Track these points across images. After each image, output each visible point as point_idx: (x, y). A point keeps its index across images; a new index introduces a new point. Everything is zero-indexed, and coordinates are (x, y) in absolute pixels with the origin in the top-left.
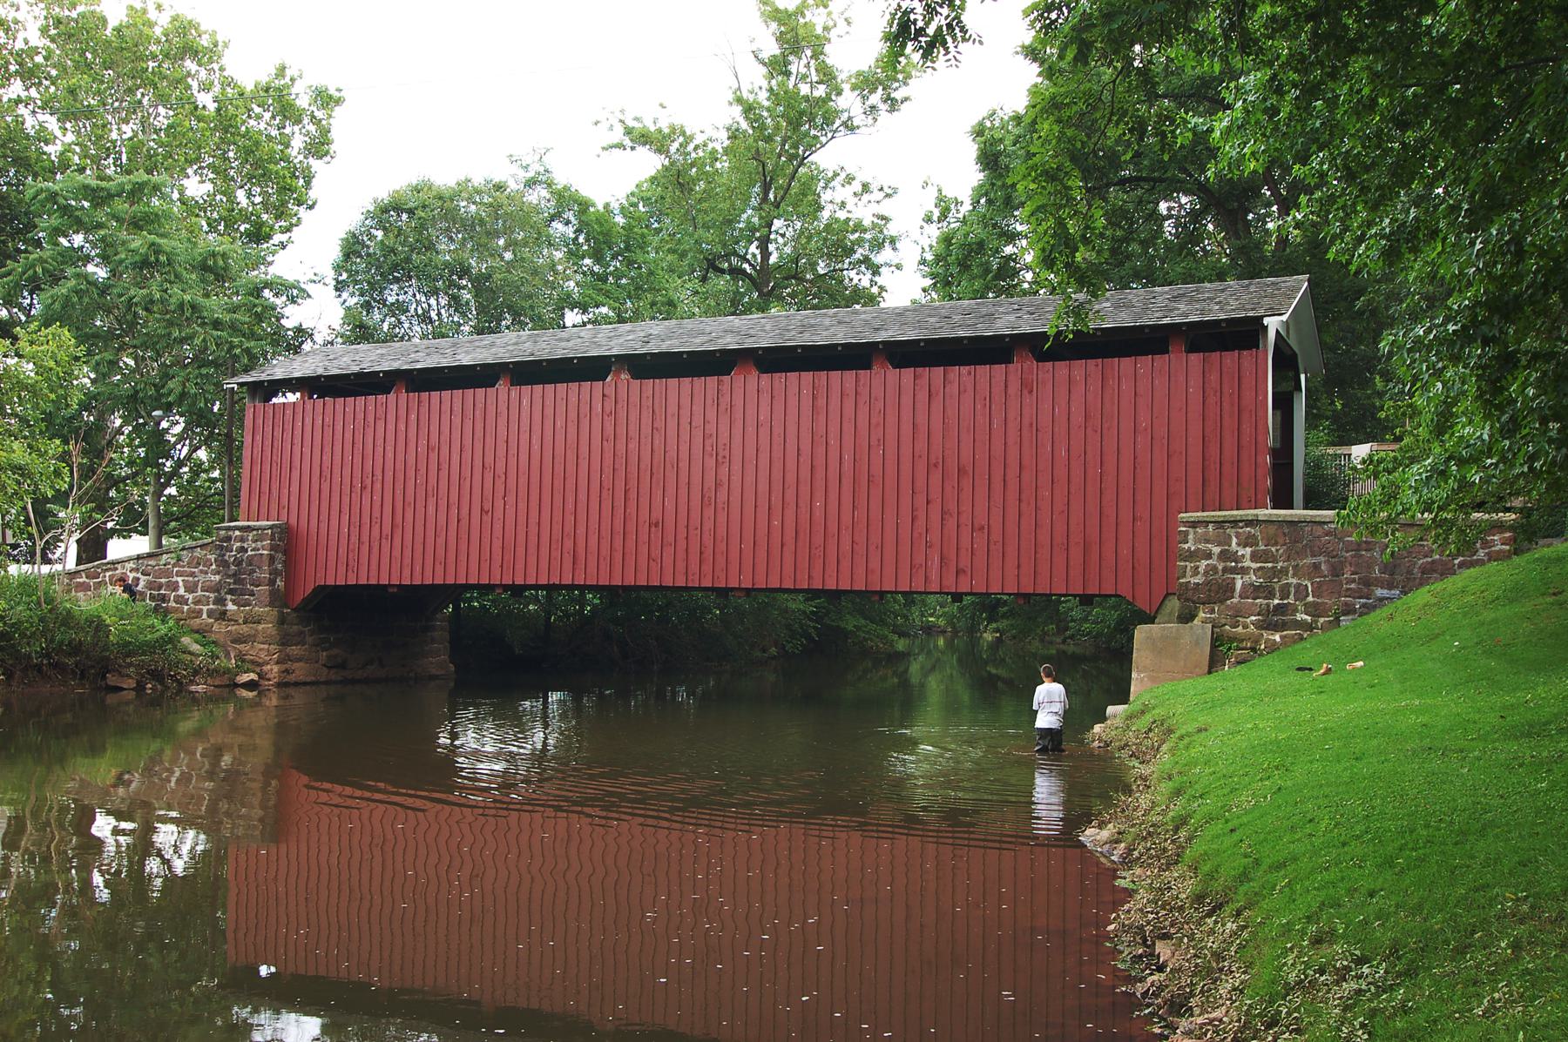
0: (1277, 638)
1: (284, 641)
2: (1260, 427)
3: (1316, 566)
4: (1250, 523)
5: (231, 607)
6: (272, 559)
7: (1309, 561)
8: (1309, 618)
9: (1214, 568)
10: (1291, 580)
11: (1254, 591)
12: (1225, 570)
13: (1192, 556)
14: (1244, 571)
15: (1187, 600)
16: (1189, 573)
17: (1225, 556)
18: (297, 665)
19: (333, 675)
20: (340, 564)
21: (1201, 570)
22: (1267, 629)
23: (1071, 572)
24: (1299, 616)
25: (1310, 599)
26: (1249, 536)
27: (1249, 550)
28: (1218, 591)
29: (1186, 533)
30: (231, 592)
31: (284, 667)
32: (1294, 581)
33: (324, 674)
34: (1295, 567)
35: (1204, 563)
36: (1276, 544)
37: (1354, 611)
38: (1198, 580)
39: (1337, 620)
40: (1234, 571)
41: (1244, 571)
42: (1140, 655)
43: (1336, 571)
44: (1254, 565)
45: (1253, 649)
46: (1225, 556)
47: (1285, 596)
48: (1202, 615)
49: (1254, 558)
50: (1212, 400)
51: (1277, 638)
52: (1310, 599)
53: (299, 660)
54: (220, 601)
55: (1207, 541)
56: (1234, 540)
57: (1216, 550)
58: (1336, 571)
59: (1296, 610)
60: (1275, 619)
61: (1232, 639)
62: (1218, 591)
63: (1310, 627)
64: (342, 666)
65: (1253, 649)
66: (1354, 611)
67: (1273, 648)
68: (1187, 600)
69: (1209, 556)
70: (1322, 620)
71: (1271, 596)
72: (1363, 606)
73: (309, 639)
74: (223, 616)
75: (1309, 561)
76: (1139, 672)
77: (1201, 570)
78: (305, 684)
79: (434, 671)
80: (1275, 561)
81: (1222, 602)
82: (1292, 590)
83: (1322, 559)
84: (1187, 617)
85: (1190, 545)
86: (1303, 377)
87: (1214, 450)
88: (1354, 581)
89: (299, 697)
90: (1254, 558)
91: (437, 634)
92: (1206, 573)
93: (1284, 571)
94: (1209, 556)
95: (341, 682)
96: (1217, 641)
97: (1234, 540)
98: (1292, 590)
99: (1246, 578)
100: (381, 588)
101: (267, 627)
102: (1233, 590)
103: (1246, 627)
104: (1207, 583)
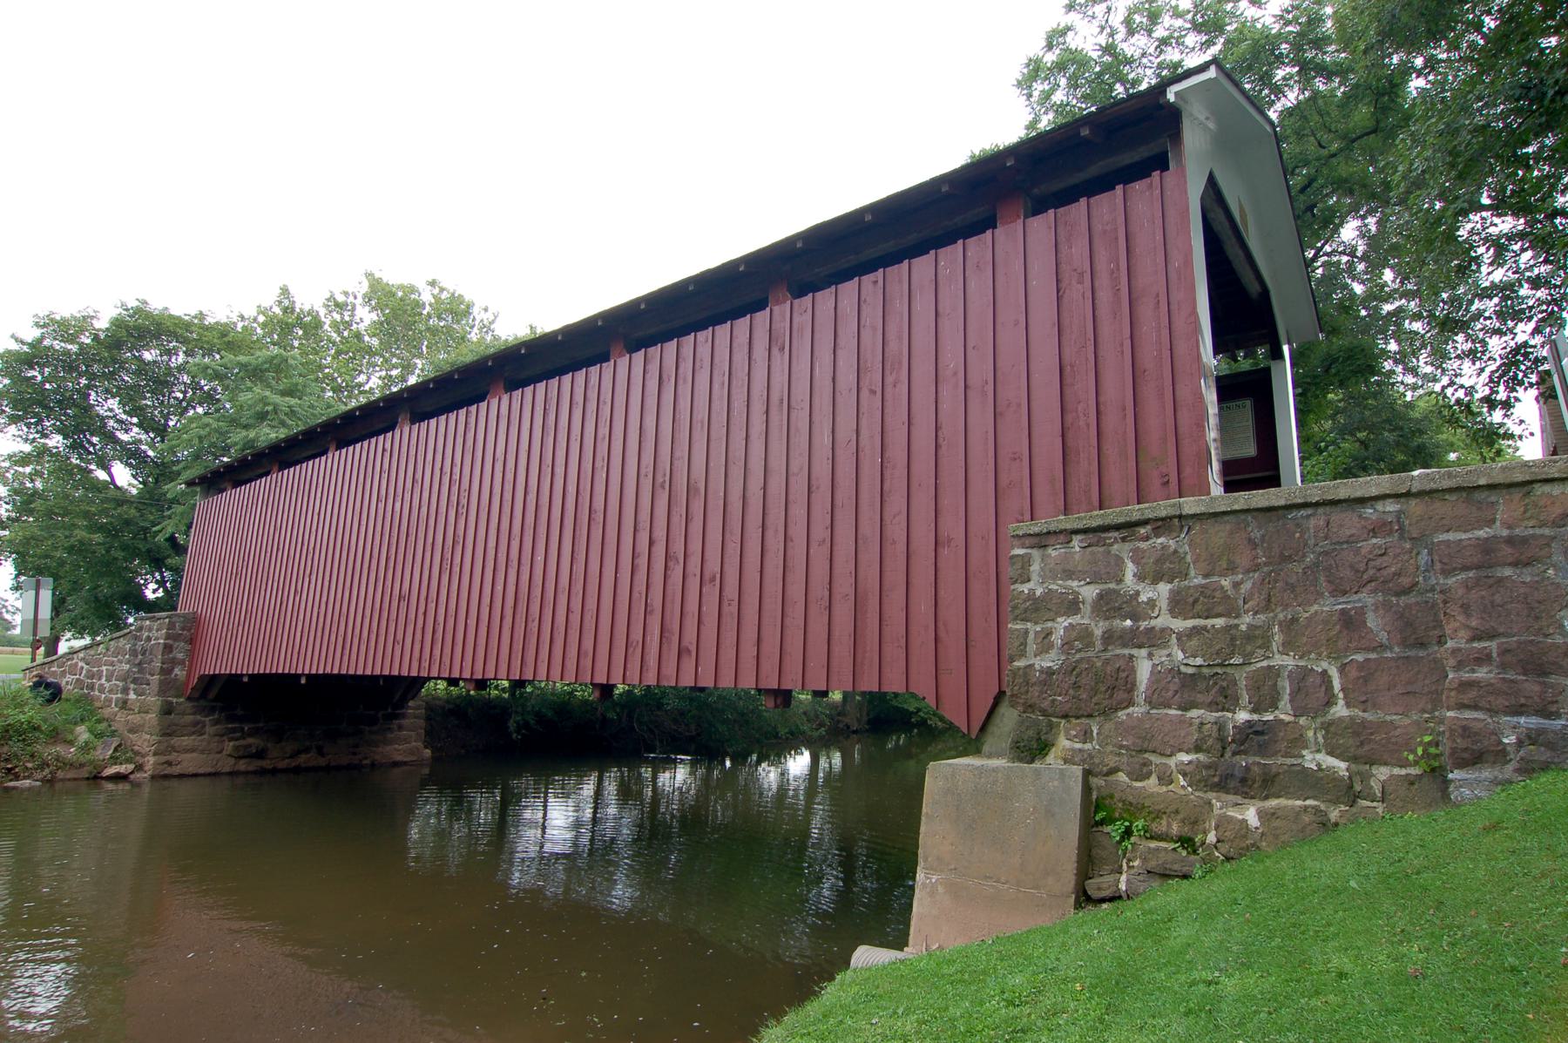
0: (1251, 815)
1: (167, 732)
2: (1180, 324)
3: (1351, 622)
4: (1161, 525)
5: (132, 696)
6: (168, 648)
7: (1327, 606)
8: (1341, 766)
9: (1085, 635)
10: (1278, 660)
11: (1184, 688)
12: (1109, 638)
13: (1038, 608)
14: (1154, 640)
15: (1030, 707)
16: (1032, 647)
17: (1109, 605)
18: (188, 756)
19: (242, 765)
20: (233, 655)
21: (1057, 638)
22: (1221, 786)
23: (836, 649)
24: (1312, 759)
25: (1340, 710)
26: (1164, 556)
27: (1164, 588)
28: (1098, 689)
29: (1026, 561)
30: (135, 681)
31: (163, 759)
32: (1289, 662)
33: (227, 765)
34: (1290, 625)
35: (1063, 622)
36: (1231, 569)
37: (1500, 755)
38: (1050, 661)
39: (1437, 774)
40: (1134, 639)
41: (1154, 640)
42: (935, 835)
43: (1417, 634)
44: (1180, 624)
45: (1187, 842)
46: (1109, 605)
47: (1265, 698)
48: (1063, 743)
49: (1179, 605)
50: (1077, 292)
51: (1251, 815)
52: (1340, 710)
53: (187, 751)
54: (125, 690)
55: (1069, 574)
56: (1130, 569)
57: (1089, 592)
58: (1417, 634)
59: (1299, 742)
60: (1245, 762)
61: (1134, 809)
62: (1098, 689)
63: (1349, 793)
64: (260, 754)
65: (1187, 842)
66: (1500, 755)
67: (1240, 846)
68: (1030, 707)
69: (1073, 606)
70: (1382, 773)
71: (1226, 700)
72: (1532, 738)
73: (210, 730)
74: (124, 705)
75: (1327, 606)
76: (930, 869)
77: (1057, 638)
78: (195, 775)
79: (399, 758)
80: (1232, 612)
81: (1107, 712)
82: (1286, 686)
83: (1366, 598)
84: (1032, 748)
85: (1034, 587)
86: (1286, 348)
87: (1083, 386)
88: (1483, 659)
89: (184, 792)
90: (1179, 605)
91: (405, 722)
92: (1067, 644)
93: (1258, 638)
94: (1073, 606)
95: (255, 773)
96: (1096, 812)
97: (1130, 569)
98: (1286, 686)
99: (1161, 656)
100: (374, 678)
101: (152, 717)
102: (1131, 686)
103: (1165, 779)
104: (1070, 669)
